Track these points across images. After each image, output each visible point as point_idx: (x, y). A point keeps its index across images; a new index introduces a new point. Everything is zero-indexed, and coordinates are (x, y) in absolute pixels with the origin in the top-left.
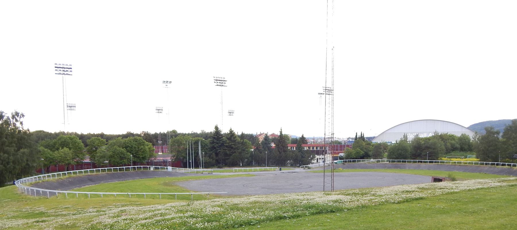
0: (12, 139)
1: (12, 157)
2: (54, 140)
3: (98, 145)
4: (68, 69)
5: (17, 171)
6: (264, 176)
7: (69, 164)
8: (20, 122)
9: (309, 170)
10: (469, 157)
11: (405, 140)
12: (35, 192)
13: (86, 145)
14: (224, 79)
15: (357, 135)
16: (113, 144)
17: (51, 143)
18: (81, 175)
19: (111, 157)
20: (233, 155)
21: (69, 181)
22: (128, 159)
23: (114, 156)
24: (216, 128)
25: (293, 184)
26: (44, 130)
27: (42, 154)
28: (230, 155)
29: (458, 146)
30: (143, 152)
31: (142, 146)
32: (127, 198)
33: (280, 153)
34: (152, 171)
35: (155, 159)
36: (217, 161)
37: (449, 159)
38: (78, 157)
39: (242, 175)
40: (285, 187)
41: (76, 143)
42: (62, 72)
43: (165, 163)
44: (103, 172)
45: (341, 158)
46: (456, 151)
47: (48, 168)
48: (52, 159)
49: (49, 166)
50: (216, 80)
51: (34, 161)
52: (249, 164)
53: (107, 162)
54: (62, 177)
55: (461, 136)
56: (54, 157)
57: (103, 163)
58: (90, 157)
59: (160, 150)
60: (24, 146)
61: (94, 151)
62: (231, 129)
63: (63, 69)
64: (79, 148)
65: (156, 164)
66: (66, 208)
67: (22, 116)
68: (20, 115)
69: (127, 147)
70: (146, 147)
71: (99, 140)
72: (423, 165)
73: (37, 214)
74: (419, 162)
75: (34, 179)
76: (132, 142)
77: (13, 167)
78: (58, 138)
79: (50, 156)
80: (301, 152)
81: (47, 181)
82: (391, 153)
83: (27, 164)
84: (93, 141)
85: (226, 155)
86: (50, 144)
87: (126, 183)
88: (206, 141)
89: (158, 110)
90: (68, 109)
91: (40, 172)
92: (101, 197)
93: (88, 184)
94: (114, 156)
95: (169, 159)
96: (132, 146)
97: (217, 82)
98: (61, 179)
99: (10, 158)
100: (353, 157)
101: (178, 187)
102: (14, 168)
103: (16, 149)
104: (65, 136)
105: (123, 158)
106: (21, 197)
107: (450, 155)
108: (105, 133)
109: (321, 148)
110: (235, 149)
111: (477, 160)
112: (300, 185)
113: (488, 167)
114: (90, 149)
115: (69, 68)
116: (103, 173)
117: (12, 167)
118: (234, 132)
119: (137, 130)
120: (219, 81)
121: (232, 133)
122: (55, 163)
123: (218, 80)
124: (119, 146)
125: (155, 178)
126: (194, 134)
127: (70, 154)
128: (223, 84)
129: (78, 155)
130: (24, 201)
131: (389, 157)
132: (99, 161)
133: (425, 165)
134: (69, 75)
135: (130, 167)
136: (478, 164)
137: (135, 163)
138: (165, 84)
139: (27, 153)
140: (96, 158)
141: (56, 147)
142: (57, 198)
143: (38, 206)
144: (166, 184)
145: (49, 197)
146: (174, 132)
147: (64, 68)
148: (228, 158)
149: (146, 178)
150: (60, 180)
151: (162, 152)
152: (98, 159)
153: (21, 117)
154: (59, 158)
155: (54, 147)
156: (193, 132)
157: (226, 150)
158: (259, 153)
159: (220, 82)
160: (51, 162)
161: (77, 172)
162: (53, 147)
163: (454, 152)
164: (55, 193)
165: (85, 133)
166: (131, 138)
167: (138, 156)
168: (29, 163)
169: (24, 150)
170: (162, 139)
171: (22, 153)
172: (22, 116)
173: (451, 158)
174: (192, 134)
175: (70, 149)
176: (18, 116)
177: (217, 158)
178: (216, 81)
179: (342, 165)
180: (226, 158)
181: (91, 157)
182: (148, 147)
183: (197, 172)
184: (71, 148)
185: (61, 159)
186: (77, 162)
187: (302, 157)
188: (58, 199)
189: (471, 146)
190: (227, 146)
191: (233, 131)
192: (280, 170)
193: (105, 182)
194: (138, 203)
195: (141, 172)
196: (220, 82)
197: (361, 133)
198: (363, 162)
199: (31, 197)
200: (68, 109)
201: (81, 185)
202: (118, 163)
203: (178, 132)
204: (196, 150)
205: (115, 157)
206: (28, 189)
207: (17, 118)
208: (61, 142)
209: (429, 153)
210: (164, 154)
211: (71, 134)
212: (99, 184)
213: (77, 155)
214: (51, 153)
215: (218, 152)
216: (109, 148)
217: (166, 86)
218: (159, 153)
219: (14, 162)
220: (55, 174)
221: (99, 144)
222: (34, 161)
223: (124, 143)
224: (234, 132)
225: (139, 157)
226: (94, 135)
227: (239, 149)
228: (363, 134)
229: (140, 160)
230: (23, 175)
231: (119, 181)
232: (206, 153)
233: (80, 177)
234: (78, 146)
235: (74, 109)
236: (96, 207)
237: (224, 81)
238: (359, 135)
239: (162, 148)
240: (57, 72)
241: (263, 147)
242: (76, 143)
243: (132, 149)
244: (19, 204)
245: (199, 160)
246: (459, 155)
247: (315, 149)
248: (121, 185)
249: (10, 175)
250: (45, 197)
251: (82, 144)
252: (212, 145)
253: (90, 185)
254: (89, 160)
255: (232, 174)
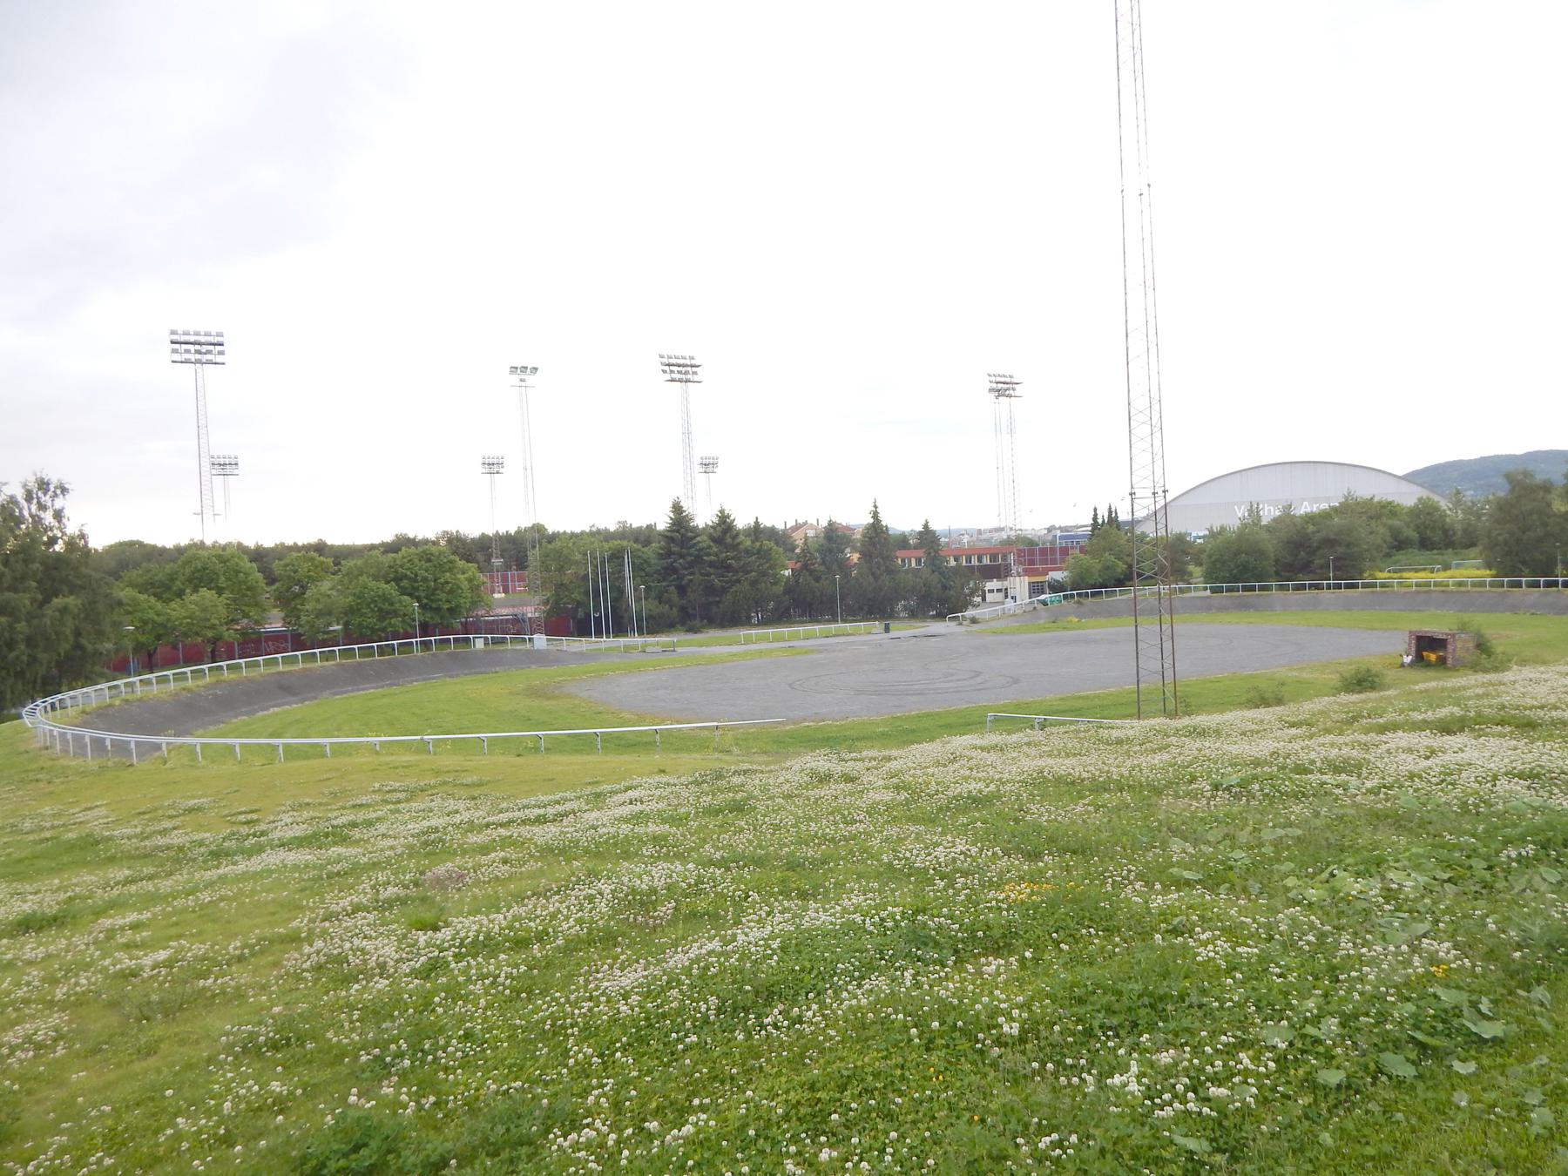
0: (27, 566)
1: (24, 623)
2: (167, 567)
3: (309, 577)
4: (211, 348)
5: (42, 671)
6: (840, 651)
7: (215, 641)
8: (55, 511)
9: (975, 627)
10: (1458, 566)
11: (1255, 524)
12: (86, 746)
13: (271, 580)
14: (693, 362)
15: (1096, 515)
16: (356, 573)
17: (160, 576)
18: (253, 673)
19: (351, 611)
20: (734, 589)
21: (215, 695)
22: (405, 615)
23: (359, 610)
24: (677, 508)
25: (952, 675)
26: (141, 540)
27: (130, 613)
28: (724, 591)
29: (1412, 534)
30: (451, 592)
31: (448, 574)
32: (424, 757)
33: (876, 578)
34: (480, 651)
35: (488, 612)
36: (683, 609)
37: (1395, 575)
38: (246, 615)
39: (772, 651)
40: (931, 687)
41: (240, 572)
42: (193, 357)
43: (518, 626)
44: (327, 660)
45: (1056, 587)
46: (1410, 550)
47: (150, 656)
48: (163, 625)
49: (153, 647)
50: (669, 365)
51: (100, 634)
52: (780, 616)
53: (339, 627)
54: (190, 683)
55: (1417, 505)
56: (168, 620)
57: (325, 633)
58: (282, 615)
59: (498, 586)
60: (65, 588)
61: (297, 596)
62: (722, 511)
63: (198, 347)
64: (249, 589)
65: (492, 627)
66: (190, 810)
67: (58, 492)
68: (52, 488)
69: (401, 579)
70: (462, 577)
71: (312, 559)
72: (1326, 595)
73: (70, 847)
74: (1311, 586)
75: (107, 691)
76: (416, 561)
77: (29, 655)
78: (183, 558)
79: (156, 617)
80: (940, 573)
81: (140, 700)
82: (1214, 563)
83: (78, 646)
84: (293, 565)
85: (710, 590)
86: (156, 578)
87: (401, 693)
88: (645, 549)
89: (489, 464)
90: (214, 472)
91: (122, 668)
92: (324, 756)
93: (279, 701)
94: (359, 610)
95: (530, 612)
96: (416, 575)
97: (672, 372)
98: (189, 690)
99: (19, 629)
100: (1092, 582)
101: (576, 702)
102: (33, 660)
103: (40, 597)
104: (205, 554)
105: (387, 613)
106: (35, 766)
107: (1395, 563)
108: (329, 542)
109: (994, 557)
110: (736, 571)
111: (1488, 572)
112: (977, 676)
113: (1536, 595)
114: (281, 590)
115: (214, 344)
116: (326, 663)
117: (25, 658)
118: (732, 518)
119: (426, 526)
120: (675, 369)
121: (724, 522)
122: (172, 639)
123: (673, 365)
124: (376, 578)
125: (496, 672)
126: (599, 532)
127: (220, 608)
128: (690, 377)
129: (246, 609)
130: (42, 780)
131: (1210, 576)
132: (313, 626)
133: (1333, 596)
134: (216, 363)
135: (414, 640)
136: (1482, 584)
137: (426, 629)
138: (515, 378)
139: (76, 611)
140: (303, 618)
141: (175, 588)
142: (165, 763)
143: (84, 806)
144: (534, 692)
145: (135, 761)
146: (538, 529)
147: (200, 344)
148: (717, 599)
149: (466, 675)
150: (184, 693)
151: (506, 591)
152: (308, 622)
153: (56, 495)
154: (185, 621)
155: (169, 588)
156: (594, 529)
157: (709, 575)
158: (813, 582)
159: (681, 371)
160: (158, 638)
161: (240, 664)
162: (165, 589)
163: (1401, 552)
164: (158, 747)
165: (268, 543)
166: (413, 550)
167: (434, 605)
168: (84, 642)
169: (66, 600)
170: (502, 551)
171: (59, 611)
172: (58, 492)
173: (1401, 571)
174: (592, 534)
175: (220, 591)
176: (46, 492)
177: (685, 602)
178: (667, 368)
179: (1075, 606)
180: (711, 599)
181: (287, 616)
182: (466, 576)
183: (627, 649)
184: (224, 588)
185: (193, 624)
186: (244, 633)
187: (945, 588)
188: (168, 766)
189: (1451, 533)
190: (711, 564)
191: (728, 516)
192: (887, 629)
193: (335, 694)
194: (469, 780)
195: (451, 655)
196: (681, 371)
197: (1110, 508)
198: (1121, 597)
199: (73, 763)
200: (214, 472)
201: (256, 707)
202: (372, 629)
203: (550, 531)
204: (618, 579)
205: (364, 611)
206: (63, 735)
207: (43, 499)
208: (193, 573)
209: (1337, 559)
210: (511, 596)
211: (224, 548)
212: (316, 701)
213: (243, 611)
214: (159, 605)
215: (684, 583)
216: (343, 585)
217: (523, 384)
218: (496, 596)
219: (30, 641)
220: (186, 673)
221: (312, 573)
222: (100, 634)
223: (391, 567)
224: (732, 518)
225: (438, 610)
226: (296, 548)
227: (751, 571)
228: (1113, 509)
229: (442, 618)
230: (65, 681)
231: (380, 690)
232: (648, 588)
233: (250, 680)
234: (245, 583)
235: (235, 472)
236: (308, 804)
237: (692, 366)
238: (1103, 514)
239: (505, 579)
240: (177, 357)
241: (823, 563)
242: (240, 572)
243: (416, 585)
244: (22, 797)
245: (626, 610)
246: (1421, 562)
247: (975, 562)
248: (386, 701)
249: (20, 683)
250: (124, 760)
251: (259, 576)
252: (664, 563)
253: (287, 704)
254: (280, 625)
255: (1460, 680)
